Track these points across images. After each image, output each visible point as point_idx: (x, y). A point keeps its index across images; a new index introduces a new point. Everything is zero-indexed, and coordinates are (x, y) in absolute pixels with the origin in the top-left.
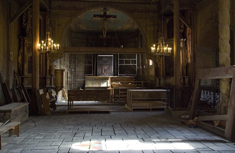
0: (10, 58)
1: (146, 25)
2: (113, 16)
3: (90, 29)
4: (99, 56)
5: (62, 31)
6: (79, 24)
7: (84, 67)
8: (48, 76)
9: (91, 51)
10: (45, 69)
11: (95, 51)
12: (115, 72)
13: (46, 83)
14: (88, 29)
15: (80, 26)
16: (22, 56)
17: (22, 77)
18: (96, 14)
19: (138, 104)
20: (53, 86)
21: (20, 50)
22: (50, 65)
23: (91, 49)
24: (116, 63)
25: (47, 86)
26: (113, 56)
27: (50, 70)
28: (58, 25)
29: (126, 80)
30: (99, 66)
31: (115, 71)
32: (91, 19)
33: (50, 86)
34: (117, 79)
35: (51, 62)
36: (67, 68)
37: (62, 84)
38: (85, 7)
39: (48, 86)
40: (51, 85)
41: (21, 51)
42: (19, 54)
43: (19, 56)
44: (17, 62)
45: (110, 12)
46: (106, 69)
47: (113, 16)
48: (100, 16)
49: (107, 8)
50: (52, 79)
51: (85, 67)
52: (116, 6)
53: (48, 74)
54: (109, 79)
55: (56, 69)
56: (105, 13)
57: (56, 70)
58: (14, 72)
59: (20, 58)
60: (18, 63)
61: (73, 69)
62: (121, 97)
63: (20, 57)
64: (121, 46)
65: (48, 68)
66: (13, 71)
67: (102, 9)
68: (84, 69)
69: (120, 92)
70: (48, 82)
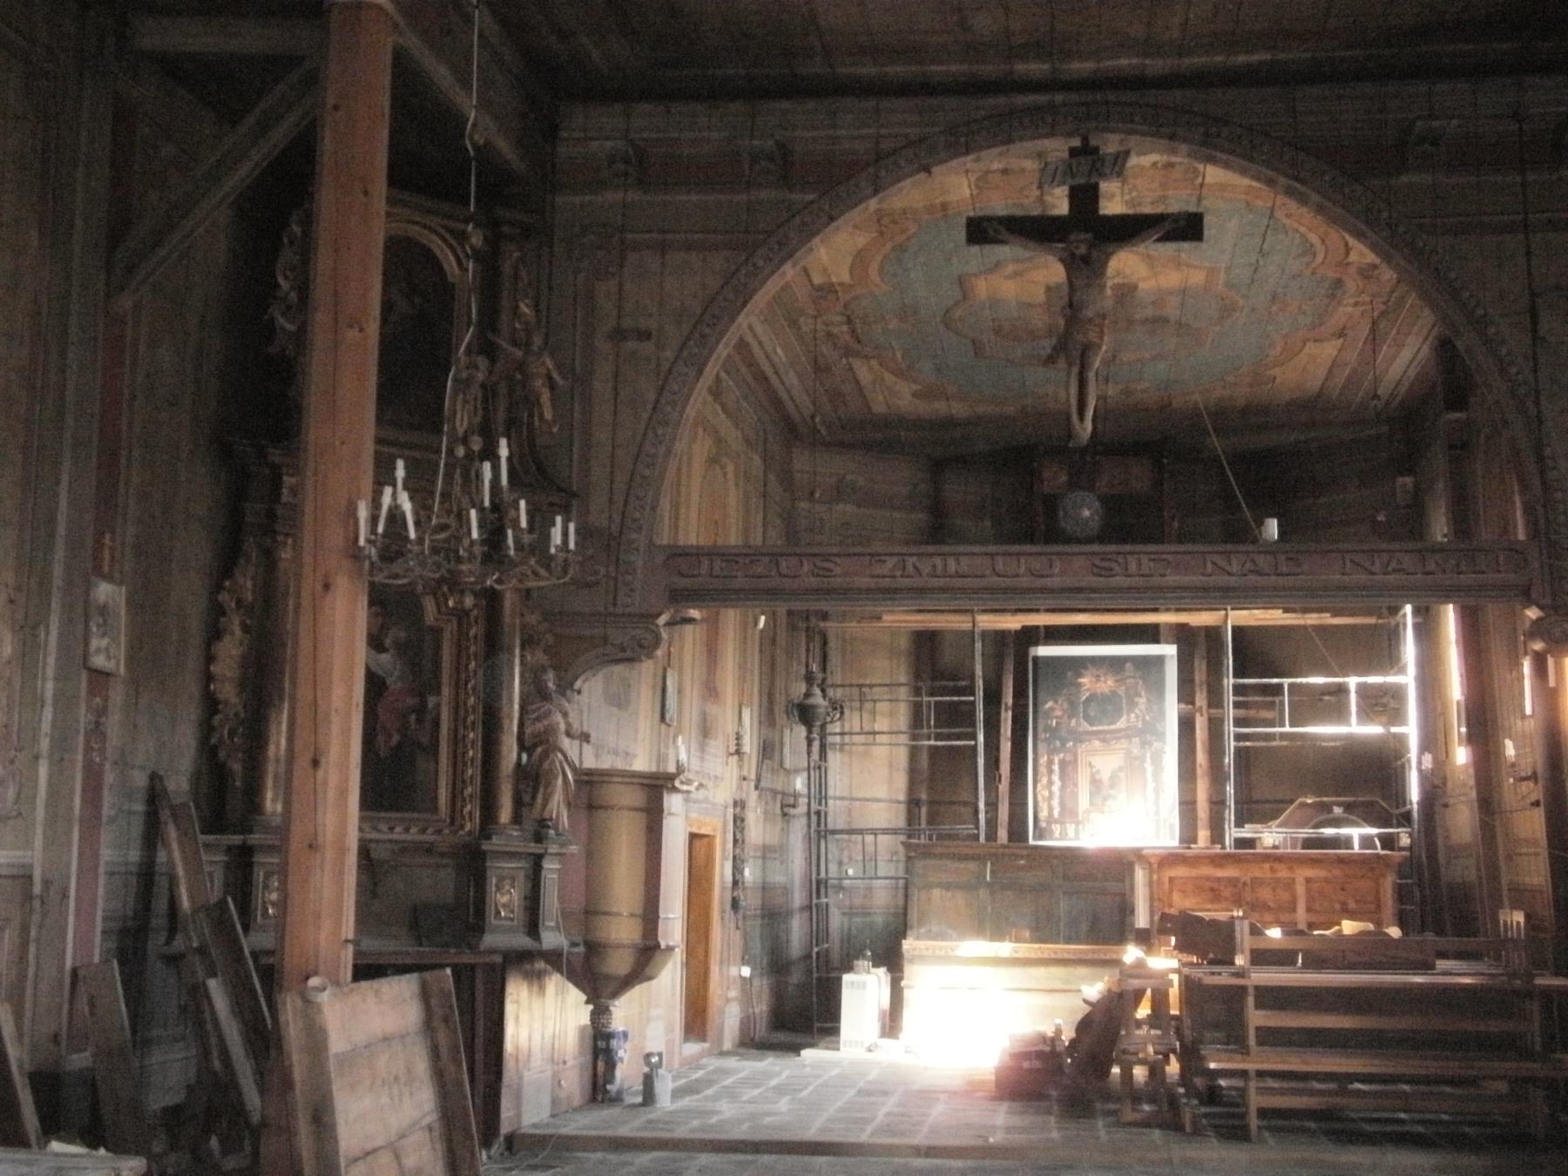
0: (87, 645)
1: (1533, 295)
2: (1168, 225)
3: (959, 410)
4: (1044, 651)
5: (652, 396)
6: (848, 352)
7: (902, 755)
8: (509, 837)
9: (936, 582)
10: (479, 762)
11: (983, 583)
12: (1194, 802)
13: (480, 912)
14: (940, 408)
15: (864, 372)
16: (246, 629)
17: (236, 839)
18: (998, 205)
19: (926, 568)
20: (552, 938)
21: (237, 572)
22: (528, 731)
23: (938, 561)
24: (1201, 724)
25: (489, 940)
26: (1169, 650)
27: (532, 779)
28: (618, 335)
29: (1308, 880)
30: (1042, 747)
31: (1194, 791)
32: (958, 294)
33: (522, 941)
34: (1220, 873)
35: (536, 694)
36: (741, 767)
37: (650, 915)
38: (885, 146)
39: (502, 935)
40: (533, 928)
41: (246, 582)
42: (224, 614)
43: (215, 633)
44: (195, 690)
45: (1142, 179)
46: (1105, 776)
47: (1168, 225)
48: (1036, 230)
49: (1110, 144)
50: (549, 865)
51: (914, 753)
52: (1196, 105)
53: (505, 815)
54: (1247, 832)
55: (590, 772)
56: (1085, 268)
57: (590, 784)
58: (155, 795)
59: (231, 650)
60: (211, 704)
61: (797, 771)
62: (1261, 1074)
63: (227, 639)
64: (1260, 523)
65: (510, 753)
66: (140, 780)
67: (1058, 148)
68: (901, 781)
69: (1256, 1018)
70: (506, 898)
